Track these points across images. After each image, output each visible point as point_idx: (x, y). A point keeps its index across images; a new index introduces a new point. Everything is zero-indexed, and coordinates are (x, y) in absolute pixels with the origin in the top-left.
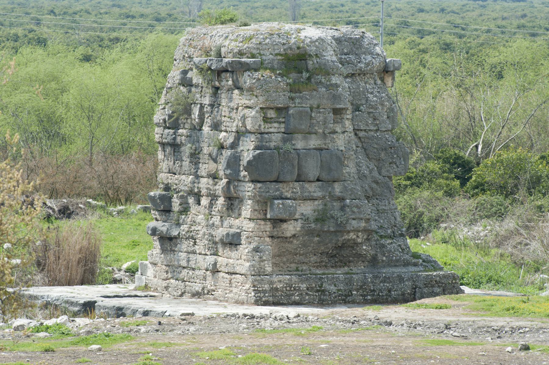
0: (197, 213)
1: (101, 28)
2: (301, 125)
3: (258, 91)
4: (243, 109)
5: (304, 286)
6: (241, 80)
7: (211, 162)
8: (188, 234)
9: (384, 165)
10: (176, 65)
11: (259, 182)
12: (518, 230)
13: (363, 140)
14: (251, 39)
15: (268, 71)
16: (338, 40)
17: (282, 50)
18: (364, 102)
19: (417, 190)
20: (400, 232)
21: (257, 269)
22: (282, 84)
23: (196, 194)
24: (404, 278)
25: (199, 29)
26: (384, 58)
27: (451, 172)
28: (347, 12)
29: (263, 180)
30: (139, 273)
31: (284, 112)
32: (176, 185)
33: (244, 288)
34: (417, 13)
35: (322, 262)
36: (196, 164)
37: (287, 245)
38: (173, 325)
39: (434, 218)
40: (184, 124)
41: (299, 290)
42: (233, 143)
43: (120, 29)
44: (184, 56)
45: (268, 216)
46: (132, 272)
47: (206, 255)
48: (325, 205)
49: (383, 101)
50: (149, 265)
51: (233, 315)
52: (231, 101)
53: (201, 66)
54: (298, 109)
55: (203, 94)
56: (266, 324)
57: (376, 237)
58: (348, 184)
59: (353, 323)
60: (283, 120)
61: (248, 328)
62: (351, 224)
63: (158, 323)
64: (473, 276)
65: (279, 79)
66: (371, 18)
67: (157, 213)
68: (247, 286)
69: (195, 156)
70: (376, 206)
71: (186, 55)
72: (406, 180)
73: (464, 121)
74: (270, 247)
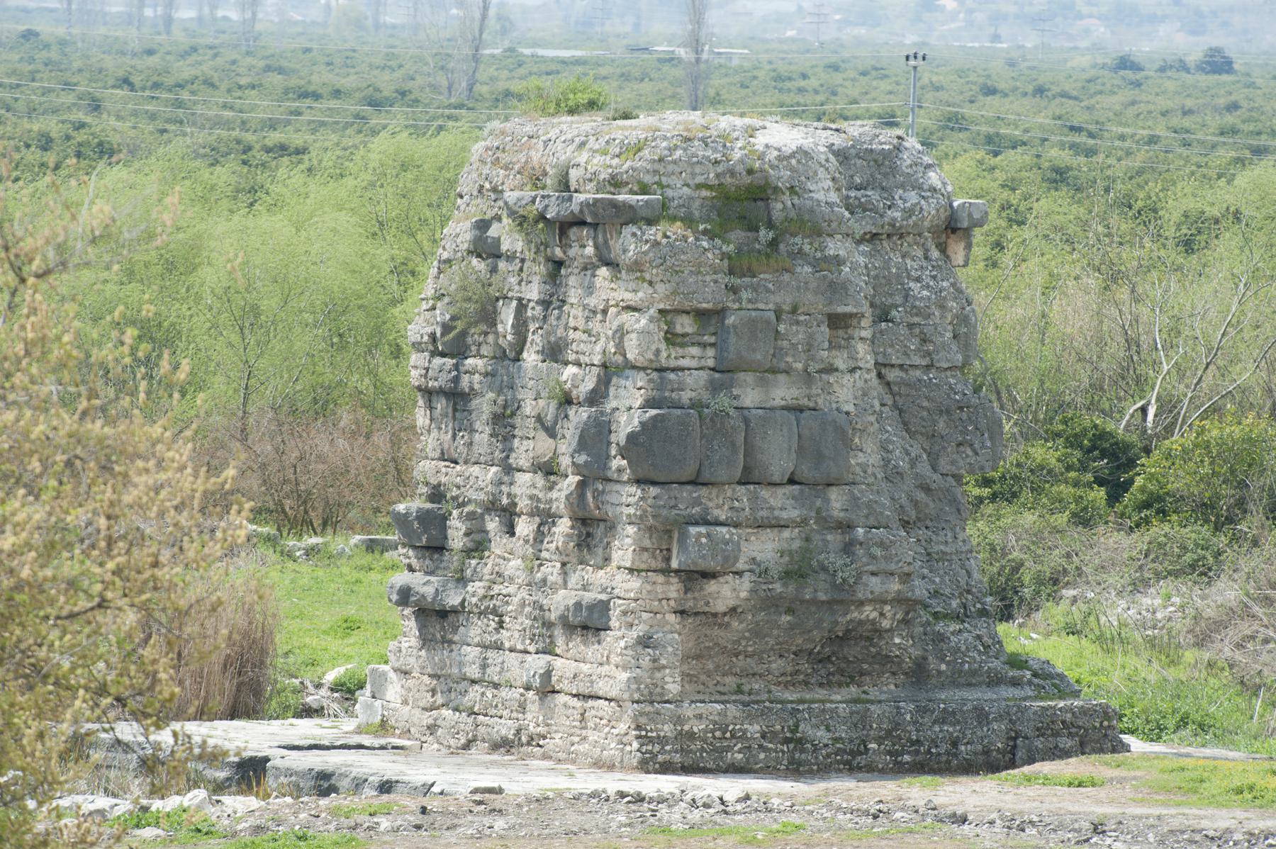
0: (506, 555)
1: (244, 123)
2: (754, 351)
3: (654, 271)
4: (619, 313)
5: (754, 729)
6: (616, 245)
7: (542, 435)
8: (486, 603)
9: (944, 448)
10: (462, 208)
11: (654, 483)
12: (1247, 606)
13: (895, 389)
14: (639, 150)
15: (678, 224)
16: (842, 155)
17: (711, 175)
18: (899, 299)
19: (1006, 509)
20: (978, 606)
21: (647, 686)
22: (710, 255)
23: (504, 510)
24: (988, 714)
25: (520, 125)
26: (949, 198)
27: (1084, 468)
28: (816, 92)
29: (662, 479)
30: (368, 690)
31: (713, 321)
32: (458, 487)
33: (615, 731)
34: (981, 98)
35: (797, 672)
36: (505, 439)
37: (716, 632)
38: (456, 816)
39: (1048, 574)
40: (480, 345)
41: (743, 737)
42: (593, 391)
43: (288, 122)
44: (482, 187)
45: (674, 564)
46: (347, 691)
47: (526, 652)
48: (807, 539)
49: (945, 298)
50: (392, 675)
51: (594, 795)
52: (591, 293)
53: (521, 212)
54: (747, 313)
55: (524, 275)
56: (673, 816)
57: (925, 616)
58: (861, 492)
59: (875, 817)
60: (713, 339)
61: (629, 825)
62: (867, 585)
63: (419, 810)
64: (1144, 711)
65: (705, 244)
66: (875, 107)
67: (411, 553)
68: (622, 727)
69: (504, 421)
70: (923, 543)
71: (487, 186)
72: (980, 487)
73: (1116, 349)
74: (676, 636)
